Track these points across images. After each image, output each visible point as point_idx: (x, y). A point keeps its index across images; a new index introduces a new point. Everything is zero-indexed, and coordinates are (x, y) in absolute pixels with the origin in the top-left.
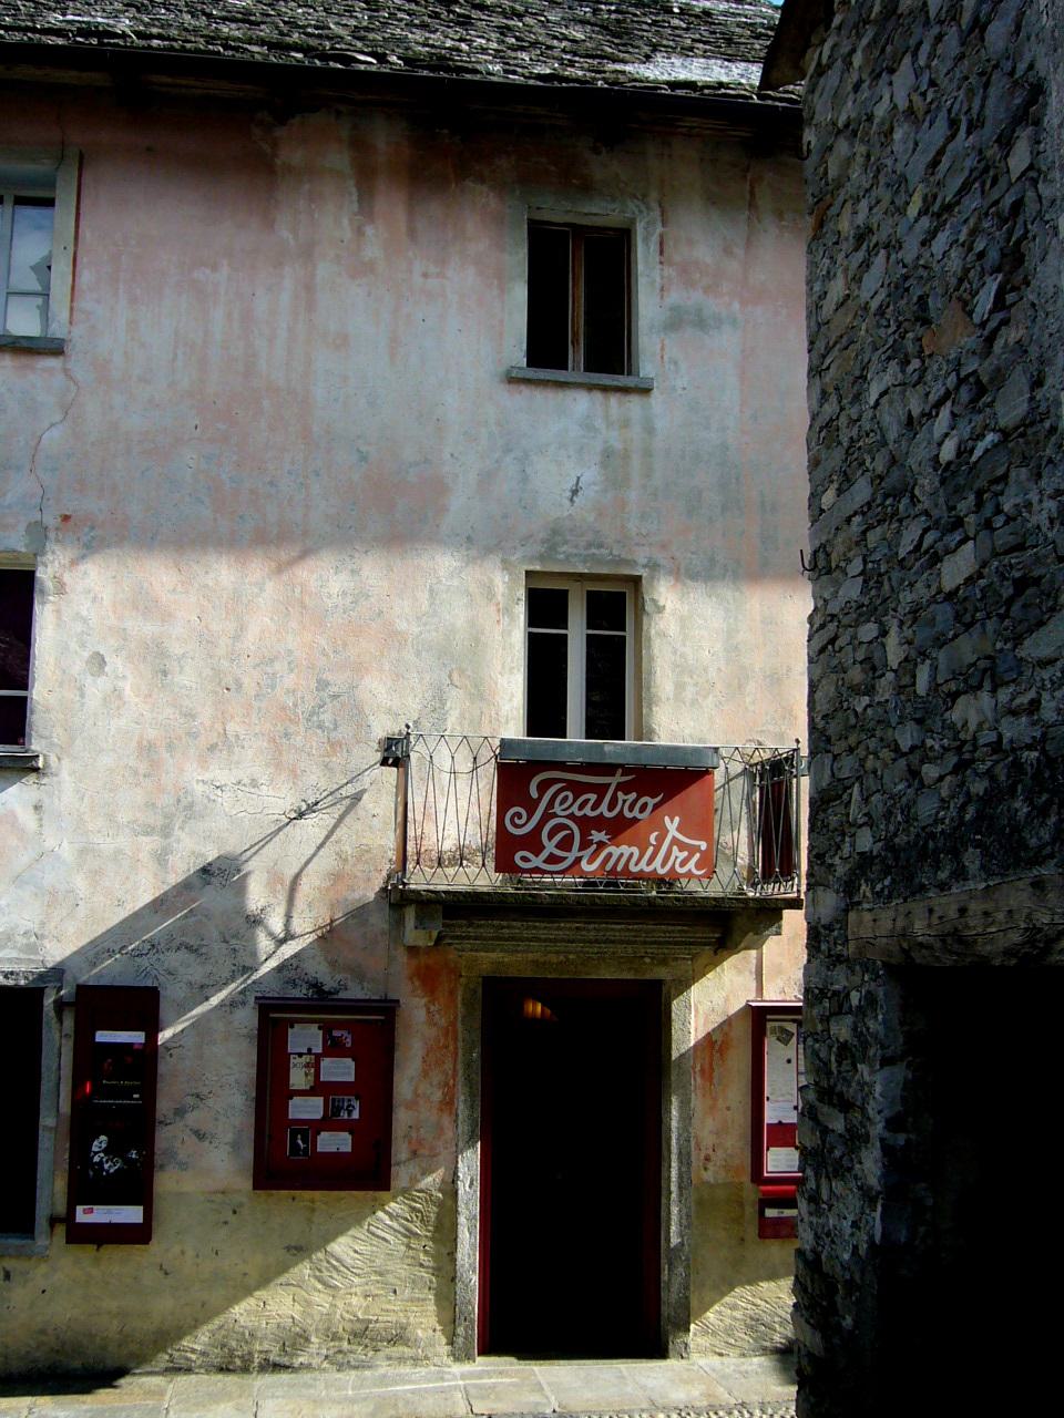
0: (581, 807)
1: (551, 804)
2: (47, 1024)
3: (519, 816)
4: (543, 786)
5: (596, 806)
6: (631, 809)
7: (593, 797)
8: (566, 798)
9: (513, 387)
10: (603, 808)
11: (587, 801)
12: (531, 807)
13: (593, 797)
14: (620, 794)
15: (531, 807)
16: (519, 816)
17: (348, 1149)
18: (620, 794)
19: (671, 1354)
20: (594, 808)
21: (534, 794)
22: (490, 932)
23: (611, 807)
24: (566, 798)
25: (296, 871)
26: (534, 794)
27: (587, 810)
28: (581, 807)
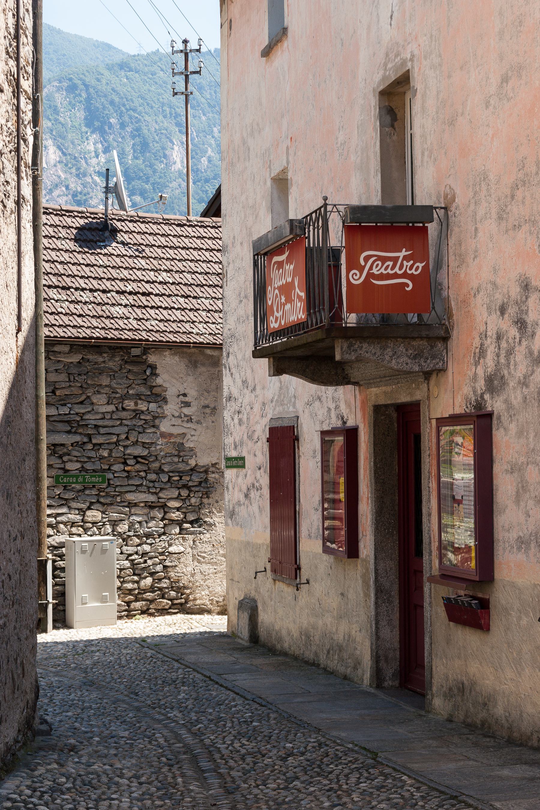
0: (386, 269)
1: (371, 268)
2: (265, 527)
3: (356, 275)
4: (366, 259)
5: (393, 268)
6: (411, 269)
7: (391, 263)
8: (378, 265)
9: (272, 56)
10: (397, 269)
11: (388, 266)
12: (361, 269)
13: (391, 263)
14: (405, 262)
15: (361, 269)
16: (356, 275)
17: (38, 636)
18: (405, 262)
19: (75, 625)
20: (392, 269)
21: (363, 263)
22: (265, 450)
23: (400, 269)
24: (378, 265)
25: (16, 313)
26: (363, 263)
27: (389, 271)
28: (386, 269)
